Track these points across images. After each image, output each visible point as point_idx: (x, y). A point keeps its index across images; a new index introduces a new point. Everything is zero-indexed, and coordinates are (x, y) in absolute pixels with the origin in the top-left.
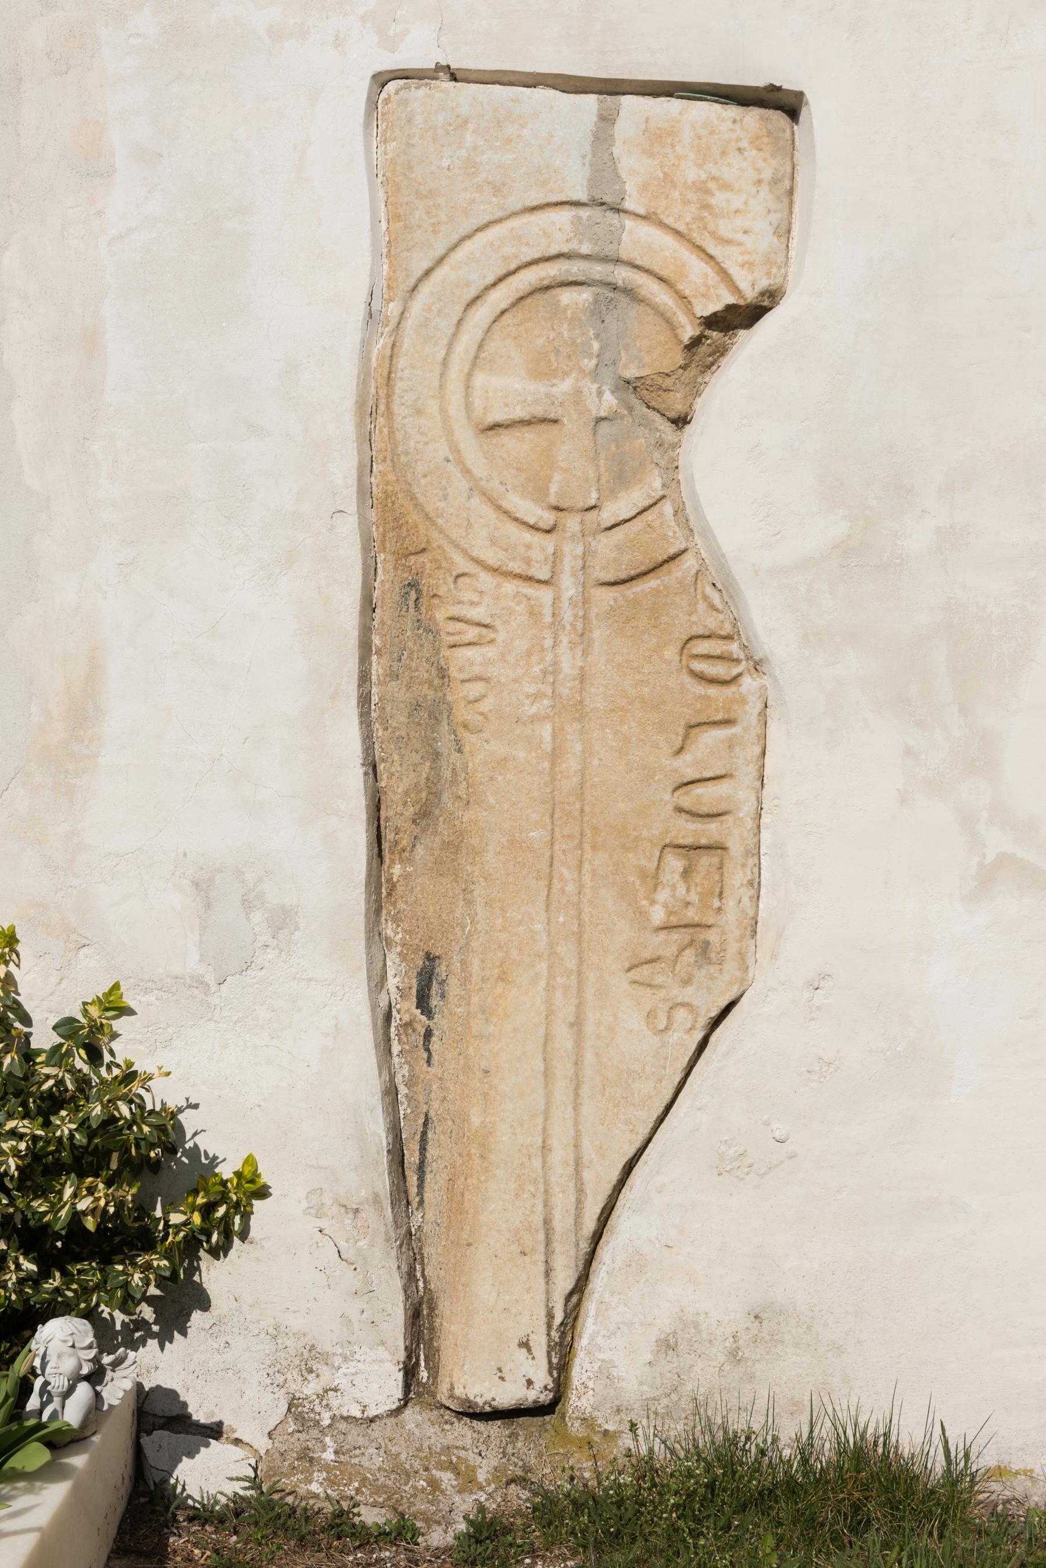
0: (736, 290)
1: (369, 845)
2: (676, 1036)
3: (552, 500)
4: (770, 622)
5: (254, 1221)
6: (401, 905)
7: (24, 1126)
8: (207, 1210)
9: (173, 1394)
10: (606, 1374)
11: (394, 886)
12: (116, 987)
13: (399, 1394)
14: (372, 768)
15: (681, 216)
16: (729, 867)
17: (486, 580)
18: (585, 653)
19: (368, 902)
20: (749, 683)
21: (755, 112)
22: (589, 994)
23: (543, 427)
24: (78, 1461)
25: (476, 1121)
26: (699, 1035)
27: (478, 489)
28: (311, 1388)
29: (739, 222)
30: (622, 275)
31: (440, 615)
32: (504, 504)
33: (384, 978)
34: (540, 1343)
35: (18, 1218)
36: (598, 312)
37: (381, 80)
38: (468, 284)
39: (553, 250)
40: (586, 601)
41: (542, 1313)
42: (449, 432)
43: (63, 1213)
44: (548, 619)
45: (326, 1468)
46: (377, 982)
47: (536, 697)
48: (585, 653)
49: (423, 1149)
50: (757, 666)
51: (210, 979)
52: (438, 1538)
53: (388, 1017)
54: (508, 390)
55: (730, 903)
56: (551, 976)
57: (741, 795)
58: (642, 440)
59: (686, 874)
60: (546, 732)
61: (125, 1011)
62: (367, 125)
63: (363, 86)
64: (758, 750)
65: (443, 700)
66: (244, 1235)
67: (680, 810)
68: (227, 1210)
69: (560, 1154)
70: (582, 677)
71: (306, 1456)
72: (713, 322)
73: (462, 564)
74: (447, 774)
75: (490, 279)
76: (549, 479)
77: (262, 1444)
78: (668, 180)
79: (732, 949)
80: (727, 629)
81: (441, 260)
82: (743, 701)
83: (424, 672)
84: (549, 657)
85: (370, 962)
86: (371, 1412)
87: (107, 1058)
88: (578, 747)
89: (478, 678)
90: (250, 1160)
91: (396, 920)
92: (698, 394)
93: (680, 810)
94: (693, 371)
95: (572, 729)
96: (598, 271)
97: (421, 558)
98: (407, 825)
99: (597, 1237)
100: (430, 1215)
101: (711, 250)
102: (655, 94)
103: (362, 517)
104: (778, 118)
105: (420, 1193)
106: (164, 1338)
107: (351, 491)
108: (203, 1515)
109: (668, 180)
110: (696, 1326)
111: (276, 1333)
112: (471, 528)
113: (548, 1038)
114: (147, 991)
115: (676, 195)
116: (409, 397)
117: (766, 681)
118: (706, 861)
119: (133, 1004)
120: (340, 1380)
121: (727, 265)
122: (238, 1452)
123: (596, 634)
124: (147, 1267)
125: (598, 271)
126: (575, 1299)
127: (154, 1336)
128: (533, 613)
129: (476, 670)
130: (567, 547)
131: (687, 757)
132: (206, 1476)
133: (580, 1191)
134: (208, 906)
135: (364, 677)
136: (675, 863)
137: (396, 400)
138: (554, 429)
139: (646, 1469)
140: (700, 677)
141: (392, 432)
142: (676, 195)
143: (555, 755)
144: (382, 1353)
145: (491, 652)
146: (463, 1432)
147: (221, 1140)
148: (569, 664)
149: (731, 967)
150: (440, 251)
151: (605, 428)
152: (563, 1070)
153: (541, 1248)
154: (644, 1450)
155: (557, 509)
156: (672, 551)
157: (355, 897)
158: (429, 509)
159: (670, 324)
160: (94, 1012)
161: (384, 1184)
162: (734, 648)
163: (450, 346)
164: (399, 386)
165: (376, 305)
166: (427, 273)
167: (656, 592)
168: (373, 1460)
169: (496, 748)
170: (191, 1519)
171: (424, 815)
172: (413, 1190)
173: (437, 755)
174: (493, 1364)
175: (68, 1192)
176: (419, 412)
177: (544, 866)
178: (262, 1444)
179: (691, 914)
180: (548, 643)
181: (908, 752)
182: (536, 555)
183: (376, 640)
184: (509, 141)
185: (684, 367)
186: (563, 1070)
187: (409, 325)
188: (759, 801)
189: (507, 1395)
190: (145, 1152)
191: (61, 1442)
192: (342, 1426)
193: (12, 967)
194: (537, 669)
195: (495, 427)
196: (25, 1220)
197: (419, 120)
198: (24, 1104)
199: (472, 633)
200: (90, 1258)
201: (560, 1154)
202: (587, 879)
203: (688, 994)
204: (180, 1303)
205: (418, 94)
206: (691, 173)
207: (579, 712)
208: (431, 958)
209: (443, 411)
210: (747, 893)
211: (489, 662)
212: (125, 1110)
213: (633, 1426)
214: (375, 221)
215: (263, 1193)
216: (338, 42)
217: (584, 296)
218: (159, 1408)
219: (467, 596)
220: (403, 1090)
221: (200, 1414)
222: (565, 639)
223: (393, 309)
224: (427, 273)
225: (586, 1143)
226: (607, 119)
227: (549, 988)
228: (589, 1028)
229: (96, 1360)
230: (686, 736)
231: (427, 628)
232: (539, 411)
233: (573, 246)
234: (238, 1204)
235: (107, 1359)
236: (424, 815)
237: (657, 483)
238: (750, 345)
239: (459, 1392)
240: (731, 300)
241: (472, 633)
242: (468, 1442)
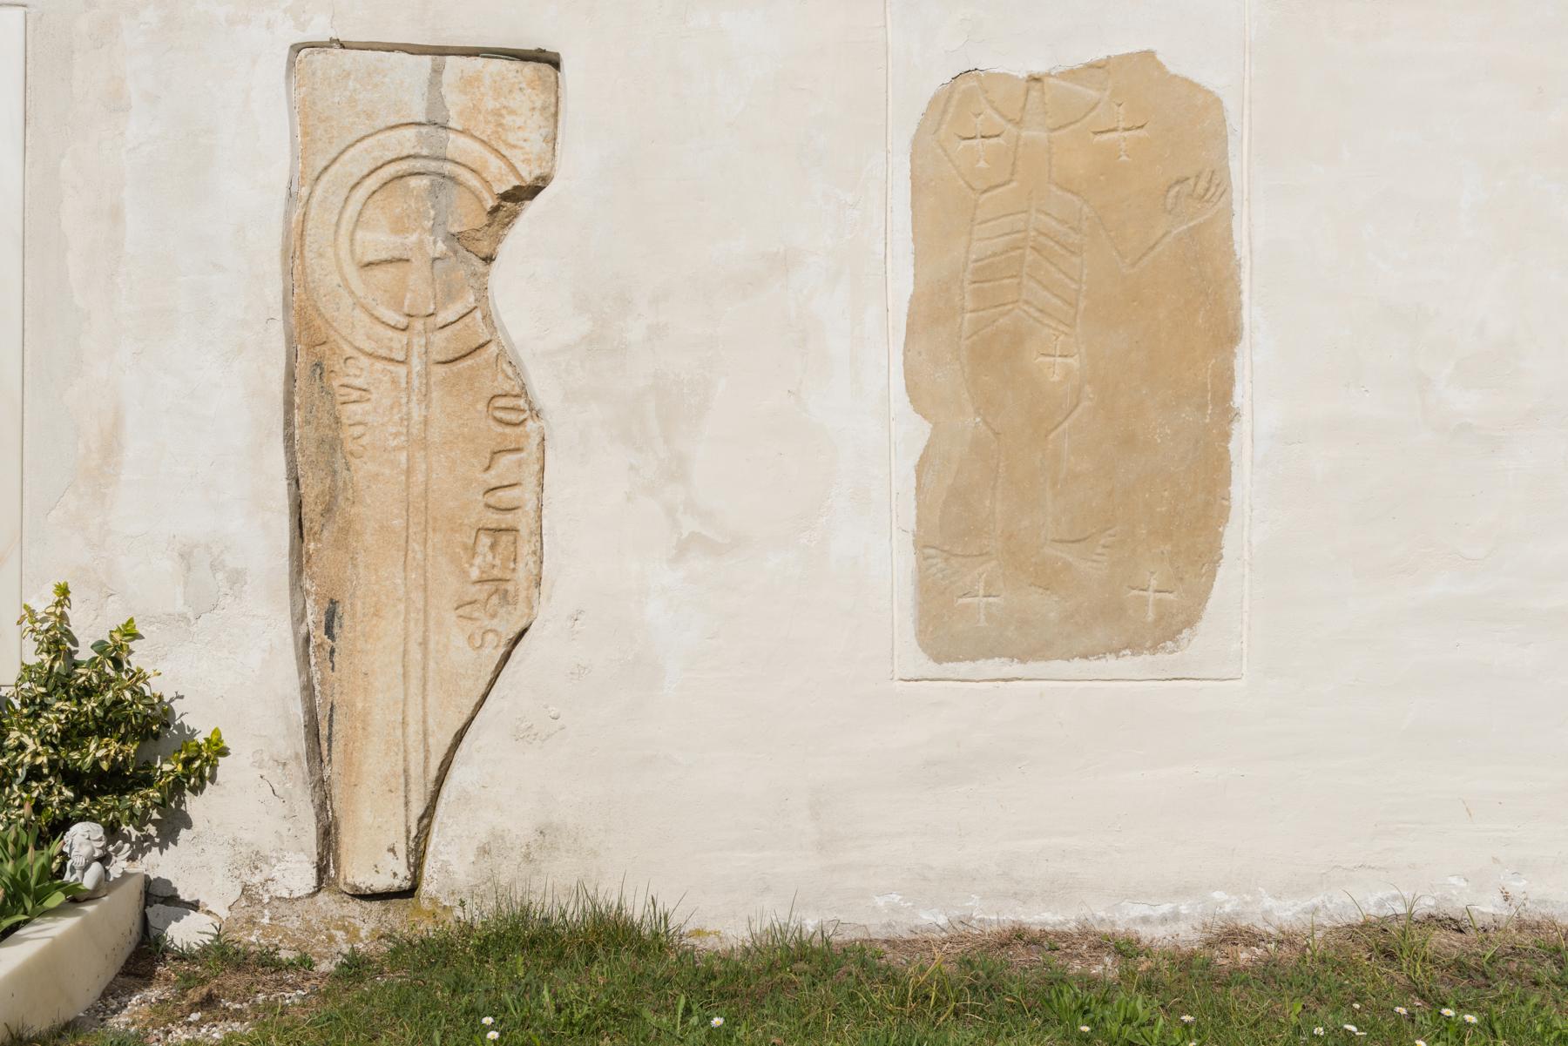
0: (519, 176)
1: (292, 530)
2: (487, 651)
3: (406, 310)
4: (543, 387)
5: (219, 771)
6: (315, 569)
7: (65, 706)
8: (187, 762)
9: (168, 883)
10: (445, 869)
11: (310, 557)
12: (131, 620)
13: (314, 883)
14: (295, 481)
15: (485, 131)
16: (520, 543)
17: (364, 361)
18: (427, 407)
19: (291, 565)
20: (530, 425)
21: (532, 65)
22: (431, 624)
23: (400, 264)
24: (90, 908)
25: (360, 705)
26: (502, 650)
27: (358, 304)
28: (257, 879)
29: (520, 134)
30: (448, 168)
31: (335, 384)
32: (376, 313)
33: (303, 616)
34: (401, 849)
35: (61, 763)
36: (433, 191)
37: (297, 48)
38: (351, 175)
39: (405, 153)
40: (427, 374)
41: (403, 829)
42: (340, 269)
43: (88, 759)
44: (404, 385)
45: (263, 928)
46: (299, 618)
47: (396, 435)
48: (427, 407)
49: (331, 726)
50: (537, 415)
51: (191, 615)
52: (325, 966)
53: (307, 640)
54: (378, 240)
55: (521, 565)
56: (407, 612)
57: (527, 496)
58: (462, 272)
59: (493, 547)
60: (403, 457)
61: (136, 636)
62: (288, 76)
63: (285, 53)
64: (537, 467)
65: (337, 438)
66: (213, 779)
67: (488, 506)
68: (201, 764)
69: (414, 727)
70: (426, 422)
71: (251, 921)
72: (506, 197)
73: (349, 351)
74: (340, 484)
75: (366, 172)
76: (404, 297)
77: (224, 914)
78: (476, 109)
79: (523, 594)
80: (517, 390)
81: (335, 160)
82: (528, 436)
83: (326, 419)
84: (404, 409)
85: (293, 604)
86: (296, 894)
87: (126, 666)
88: (424, 467)
89: (360, 423)
90: (216, 731)
91: (312, 578)
92: (499, 242)
93: (488, 506)
94: (495, 228)
95: (419, 455)
96: (433, 165)
97: (323, 348)
98: (318, 517)
99: (440, 781)
100: (335, 769)
101: (504, 152)
102: (469, 55)
103: (286, 322)
104: (546, 69)
105: (329, 755)
106: (163, 847)
107: (279, 306)
108: (181, 957)
109: (476, 109)
110: (503, 838)
111: (234, 843)
112: (355, 326)
113: (405, 652)
114: (151, 623)
115: (481, 117)
116: (315, 246)
117: (543, 423)
118: (505, 539)
119: (141, 632)
120: (276, 874)
121: (513, 161)
122: (209, 919)
123: (434, 395)
124: (147, 797)
125: (433, 165)
126: (425, 821)
127: (156, 845)
128: (394, 382)
129: (358, 418)
130: (416, 340)
131: (492, 472)
132: (185, 932)
133: (427, 751)
134: (189, 569)
135: (288, 423)
136: (485, 540)
137: (307, 248)
138: (406, 265)
139: (467, 929)
140: (500, 421)
141: (304, 269)
142: (481, 117)
143: (409, 472)
144: (302, 856)
145: (367, 406)
146: (355, 908)
147: (197, 719)
148: (417, 414)
149: (522, 607)
150: (334, 155)
151: (438, 264)
152: (415, 673)
153: (402, 788)
154: (468, 917)
155: (410, 316)
156: (481, 341)
157: (283, 563)
158: (328, 316)
159: (480, 200)
160: (117, 636)
161: (302, 747)
162: (521, 403)
163: (341, 213)
164: (308, 240)
165: (294, 189)
166: (326, 168)
167: (471, 368)
168: (294, 924)
169: (371, 467)
170: (175, 959)
171: (328, 511)
172: (325, 753)
173: (335, 472)
174: (372, 861)
175: (93, 746)
176: (321, 255)
177: (402, 542)
178: (224, 914)
179: (496, 573)
180: (404, 400)
181: (632, 467)
182: (395, 345)
183: (297, 400)
184: (376, 86)
185: (489, 225)
186: (415, 673)
187: (314, 201)
188: (540, 500)
189: (381, 883)
190: (151, 724)
191: (77, 898)
192: (276, 903)
193: (66, 609)
194: (396, 418)
195: (369, 264)
196: (66, 764)
197: (319, 73)
198: (67, 692)
199: (355, 395)
200: (113, 793)
201: (414, 727)
202: (430, 551)
203: (494, 624)
204: (172, 824)
205: (319, 57)
206: (490, 104)
207: (424, 444)
208: (333, 602)
209: (336, 255)
210: (531, 560)
211: (366, 413)
212: (128, 695)
213: (462, 903)
214: (293, 136)
215: (224, 752)
216: (269, 25)
217: (425, 182)
218: (160, 891)
219: (353, 371)
220: (318, 688)
221: (185, 896)
222: (414, 398)
223: (305, 191)
224: (326, 168)
225: (430, 721)
226: (437, 71)
227: (406, 620)
228: (432, 646)
229: (104, 848)
230: (492, 459)
231: (327, 391)
232: (397, 254)
233: (417, 150)
234: (208, 759)
235: (111, 848)
236: (328, 511)
237: (472, 299)
238: (532, 209)
239: (349, 880)
240: (517, 183)
241: (355, 395)
242: (357, 914)
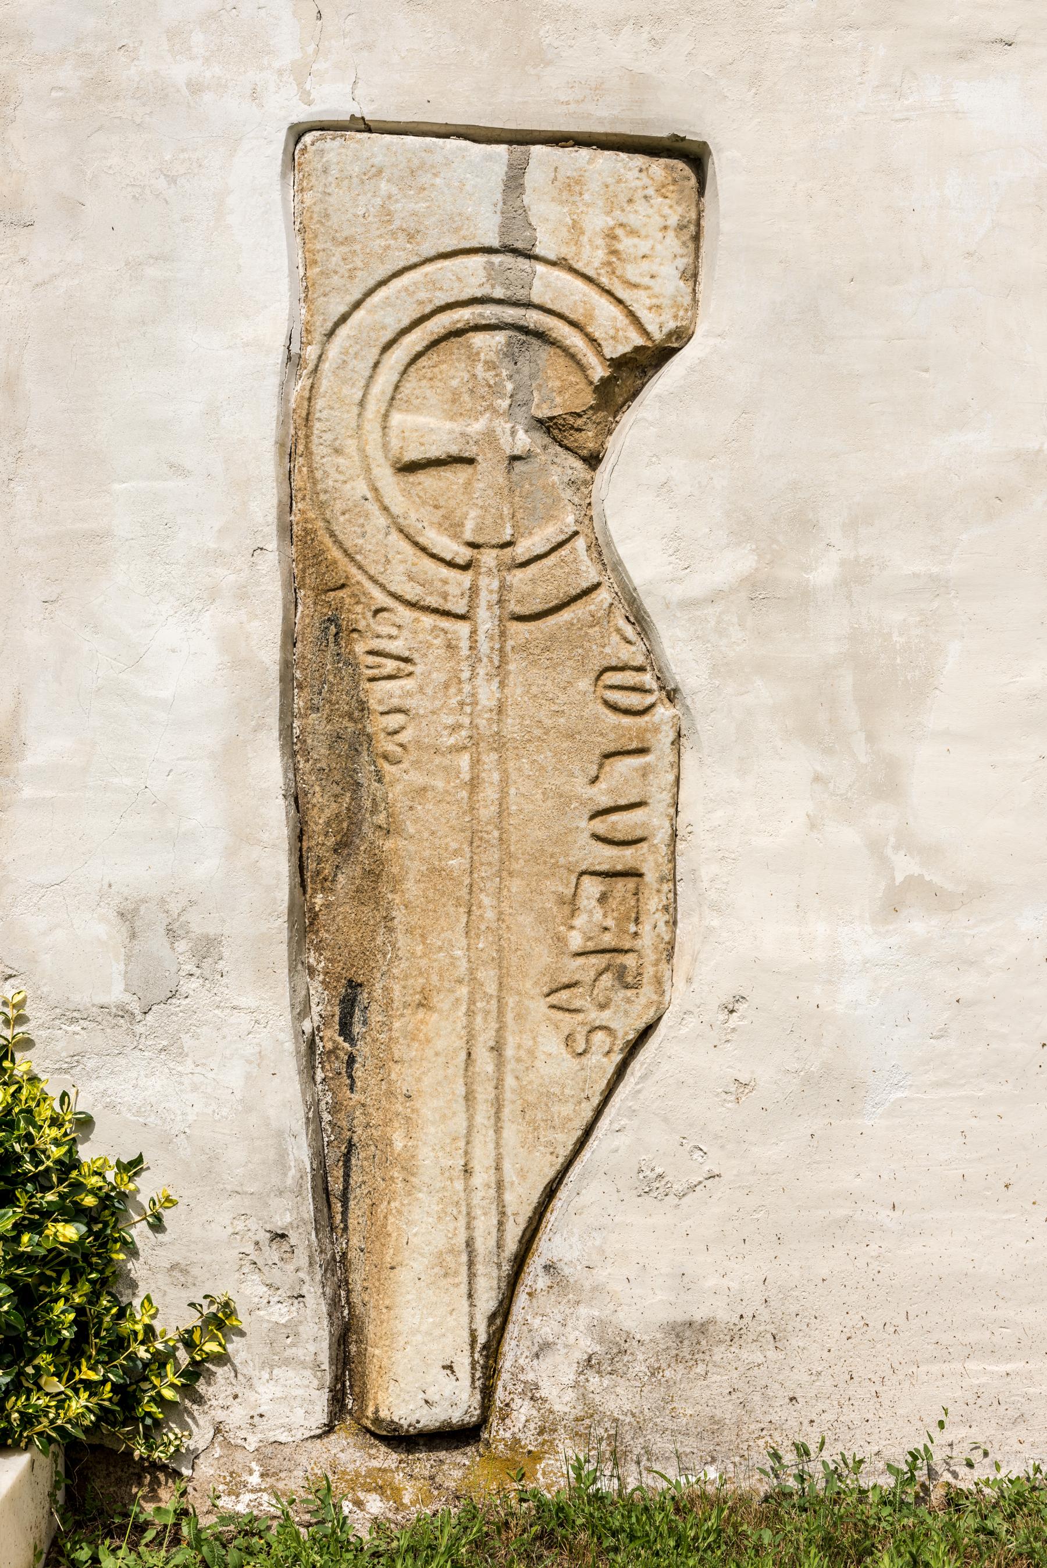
96: (510, 314)
125: (510, 314)
226: (515, 181)
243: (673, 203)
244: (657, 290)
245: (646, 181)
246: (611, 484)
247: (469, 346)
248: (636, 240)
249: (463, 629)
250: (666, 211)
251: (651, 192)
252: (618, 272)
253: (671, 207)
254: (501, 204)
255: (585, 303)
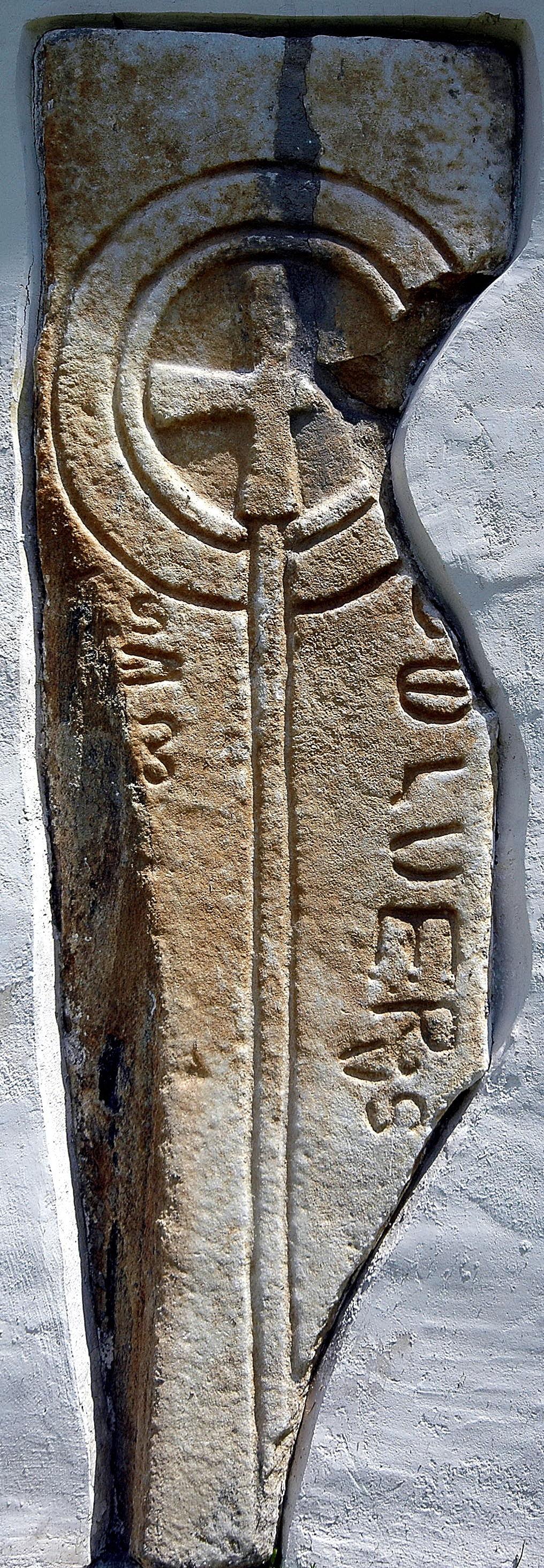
96: (290, 240)
115: (378, 148)
125: (290, 240)
226: (295, 63)
243: (484, 98)
244: (466, 203)
245: (452, 73)
246: (417, 441)
247: (244, 282)
248: (440, 146)
249: (241, 618)
250: (478, 109)
251: (458, 86)
252: (420, 184)
253: (482, 104)
254: (276, 107)
255: (379, 222)
